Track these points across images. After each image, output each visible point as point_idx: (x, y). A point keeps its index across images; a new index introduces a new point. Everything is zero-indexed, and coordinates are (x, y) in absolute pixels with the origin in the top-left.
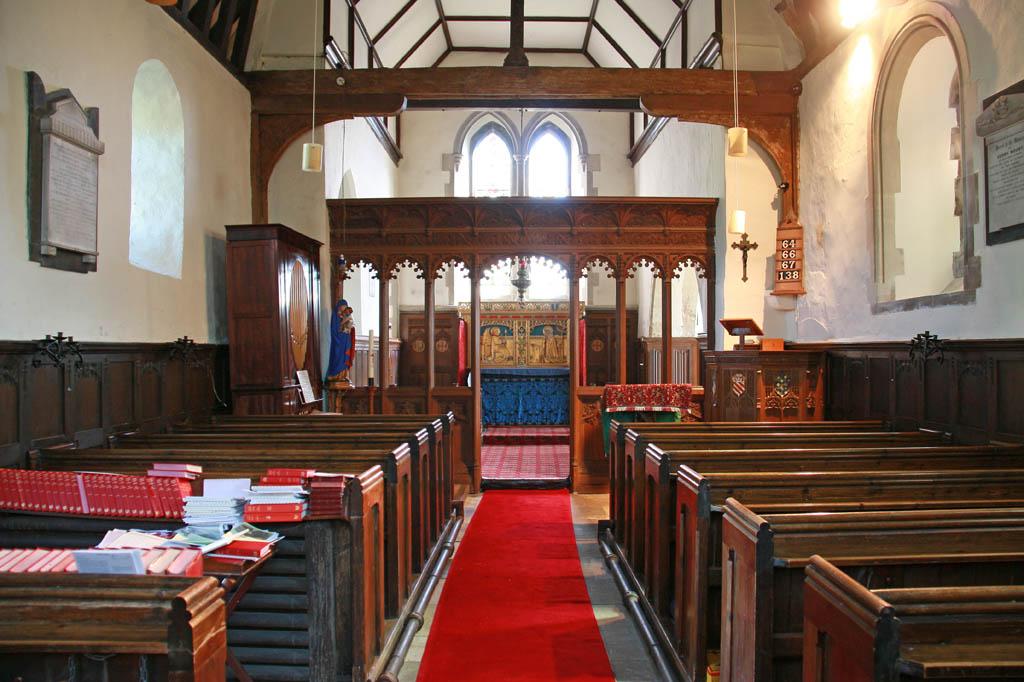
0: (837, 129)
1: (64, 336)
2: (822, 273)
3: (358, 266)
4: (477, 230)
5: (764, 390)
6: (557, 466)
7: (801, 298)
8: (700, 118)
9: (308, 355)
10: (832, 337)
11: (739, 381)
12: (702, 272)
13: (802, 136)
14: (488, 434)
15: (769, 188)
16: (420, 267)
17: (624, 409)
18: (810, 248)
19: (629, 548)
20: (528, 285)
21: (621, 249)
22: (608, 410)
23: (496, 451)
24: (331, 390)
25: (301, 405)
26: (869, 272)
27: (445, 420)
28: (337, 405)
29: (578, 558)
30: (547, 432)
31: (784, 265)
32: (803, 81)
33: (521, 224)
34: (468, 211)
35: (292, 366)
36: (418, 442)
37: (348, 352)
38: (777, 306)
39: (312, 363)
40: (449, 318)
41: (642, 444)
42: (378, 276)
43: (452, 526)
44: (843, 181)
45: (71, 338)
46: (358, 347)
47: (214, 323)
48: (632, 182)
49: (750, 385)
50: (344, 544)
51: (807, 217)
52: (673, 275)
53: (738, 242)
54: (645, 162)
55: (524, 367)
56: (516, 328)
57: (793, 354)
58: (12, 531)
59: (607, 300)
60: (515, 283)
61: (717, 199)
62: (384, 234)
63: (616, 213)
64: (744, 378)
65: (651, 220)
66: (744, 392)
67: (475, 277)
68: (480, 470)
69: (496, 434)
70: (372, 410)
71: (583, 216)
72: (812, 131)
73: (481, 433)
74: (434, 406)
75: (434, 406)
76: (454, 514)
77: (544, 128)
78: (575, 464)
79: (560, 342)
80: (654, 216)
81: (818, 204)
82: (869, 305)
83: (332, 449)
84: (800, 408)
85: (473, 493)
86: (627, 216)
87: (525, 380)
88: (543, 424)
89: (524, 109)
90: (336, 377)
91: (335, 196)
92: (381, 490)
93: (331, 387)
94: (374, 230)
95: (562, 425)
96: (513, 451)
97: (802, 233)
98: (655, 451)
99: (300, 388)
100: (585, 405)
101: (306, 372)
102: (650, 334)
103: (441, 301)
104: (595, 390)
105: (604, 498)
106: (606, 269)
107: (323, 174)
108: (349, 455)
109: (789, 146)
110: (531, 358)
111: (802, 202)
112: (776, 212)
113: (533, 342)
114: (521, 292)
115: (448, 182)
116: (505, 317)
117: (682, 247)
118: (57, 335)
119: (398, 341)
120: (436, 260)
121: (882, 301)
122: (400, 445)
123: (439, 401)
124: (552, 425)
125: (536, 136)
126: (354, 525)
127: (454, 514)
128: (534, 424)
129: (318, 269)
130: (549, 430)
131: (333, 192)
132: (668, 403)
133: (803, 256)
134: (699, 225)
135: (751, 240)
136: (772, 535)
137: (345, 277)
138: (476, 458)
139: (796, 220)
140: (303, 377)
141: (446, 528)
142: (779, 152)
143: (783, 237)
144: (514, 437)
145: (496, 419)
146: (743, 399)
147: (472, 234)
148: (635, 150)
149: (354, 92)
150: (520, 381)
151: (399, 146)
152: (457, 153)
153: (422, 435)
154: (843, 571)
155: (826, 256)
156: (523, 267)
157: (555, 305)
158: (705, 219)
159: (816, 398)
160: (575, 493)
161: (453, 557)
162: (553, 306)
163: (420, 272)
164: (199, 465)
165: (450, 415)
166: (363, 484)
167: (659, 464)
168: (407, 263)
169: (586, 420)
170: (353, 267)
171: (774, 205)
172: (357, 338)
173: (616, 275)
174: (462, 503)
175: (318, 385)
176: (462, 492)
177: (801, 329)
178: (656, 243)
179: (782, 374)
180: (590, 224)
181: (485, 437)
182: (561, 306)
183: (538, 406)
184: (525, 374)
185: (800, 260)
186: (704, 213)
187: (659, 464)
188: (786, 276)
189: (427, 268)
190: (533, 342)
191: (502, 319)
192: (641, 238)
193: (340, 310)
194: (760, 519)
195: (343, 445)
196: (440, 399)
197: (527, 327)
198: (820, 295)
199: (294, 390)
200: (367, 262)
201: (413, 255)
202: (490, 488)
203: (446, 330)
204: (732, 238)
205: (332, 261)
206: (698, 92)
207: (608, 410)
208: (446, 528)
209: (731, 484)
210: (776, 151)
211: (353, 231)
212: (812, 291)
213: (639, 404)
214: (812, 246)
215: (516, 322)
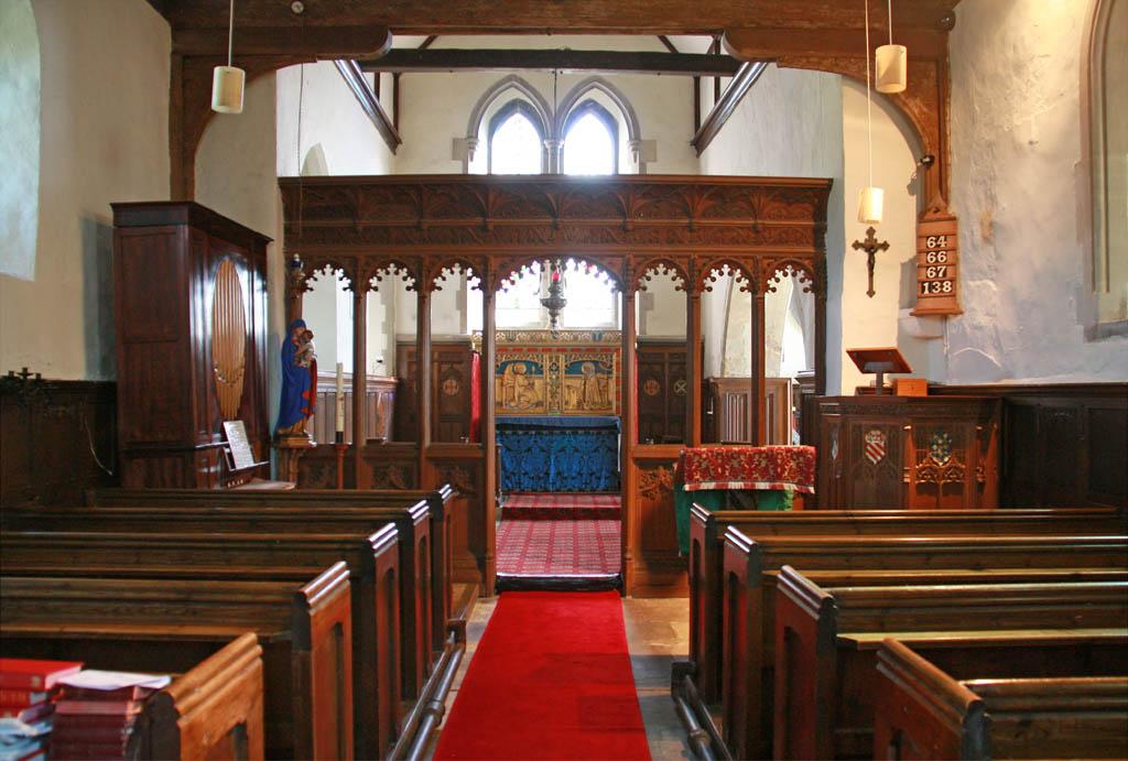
0: (1018, 68)
1: (29, 371)
2: (991, 283)
4: (492, 222)
5: (914, 455)
6: (602, 555)
7: (954, 321)
8: (808, 62)
9: (244, 399)
10: (1010, 376)
11: (874, 440)
12: (808, 283)
13: (954, 88)
14: (509, 506)
15: (904, 164)
16: (410, 274)
17: (711, 485)
18: (969, 246)
19: (730, 725)
20: (563, 306)
21: (698, 249)
22: (687, 487)
25: (230, 473)
26: (1080, 277)
28: (291, 470)
29: (643, 731)
30: (586, 502)
31: (931, 273)
32: (957, 9)
33: (553, 214)
34: (480, 198)
35: (213, 416)
36: (413, 520)
37: (306, 396)
39: (251, 410)
40: (455, 353)
42: (352, 287)
44: (1031, 143)
45: (38, 375)
46: (321, 388)
47: (97, 351)
48: (698, 166)
49: (893, 448)
51: (964, 198)
52: (767, 288)
53: (862, 241)
55: (557, 414)
56: (547, 365)
57: (946, 404)
59: (672, 327)
60: (546, 303)
61: (831, 180)
62: (360, 228)
64: (884, 437)
65: (736, 209)
66: (883, 458)
68: (494, 564)
69: (520, 505)
70: (341, 485)
71: (642, 202)
73: (497, 502)
74: (430, 472)
75: (430, 472)
76: (450, 641)
77: (584, 107)
79: (603, 383)
82: (1081, 328)
84: (966, 482)
85: (484, 596)
87: (558, 432)
88: (581, 490)
89: (558, 71)
90: (290, 429)
93: (283, 444)
95: (606, 491)
96: (542, 528)
97: (955, 226)
98: (739, 539)
99: (228, 446)
100: (642, 472)
101: (241, 422)
102: (722, 373)
103: (442, 326)
104: (653, 450)
106: (674, 279)
111: (954, 182)
112: (915, 197)
113: (569, 383)
114: (554, 315)
116: (532, 350)
117: (780, 249)
118: (21, 371)
119: (392, 380)
120: (433, 264)
121: (1104, 320)
122: (330, 565)
123: (437, 465)
124: (593, 492)
125: (573, 117)
127: (450, 641)
128: (570, 490)
129: (263, 275)
130: (589, 499)
132: (779, 477)
133: (957, 259)
134: (803, 217)
135: (880, 238)
138: (489, 546)
139: (946, 208)
140: (234, 432)
142: (922, 113)
143: (928, 233)
145: (520, 483)
147: (484, 228)
149: (316, 24)
150: (552, 434)
151: (397, 129)
152: (472, 137)
153: (419, 510)
154: (922, 656)
155: (998, 257)
156: (556, 281)
157: (597, 335)
158: (811, 209)
159: (987, 469)
160: (629, 597)
161: (441, 727)
162: (594, 336)
163: (410, 282)
165: (446, 492)
167: (705, 526)
168: (392, 268)
169: (645, 494)
170: (317, 273)
171: (911, 189)
173: (687, 287)
174: (464, 623)
175: (261, 441)
177: (952, 365)
178: (745, 242)
180: (649, 215)
181: (504, 508)
183: (575, 467)
184: (558, 424)
185: (954, 265)
187: (817, 617)
188: (932, 290)
189: (421, 275)
191: (527, 352)
193: (296, 334)
194: (823, 593)
196: (437, 461)
197: (562, 364)
198: (987, 314)
199: (217, 450)
201: (400, 257)
203: (455, 366)
204: (854, 232)
206: (806, 25)
207: (687, 487)
208: (437, 668)
211: (310, 223)
212: (974, 310)
213: (735, 478)
214: (973, 245)
215: (546, 356)
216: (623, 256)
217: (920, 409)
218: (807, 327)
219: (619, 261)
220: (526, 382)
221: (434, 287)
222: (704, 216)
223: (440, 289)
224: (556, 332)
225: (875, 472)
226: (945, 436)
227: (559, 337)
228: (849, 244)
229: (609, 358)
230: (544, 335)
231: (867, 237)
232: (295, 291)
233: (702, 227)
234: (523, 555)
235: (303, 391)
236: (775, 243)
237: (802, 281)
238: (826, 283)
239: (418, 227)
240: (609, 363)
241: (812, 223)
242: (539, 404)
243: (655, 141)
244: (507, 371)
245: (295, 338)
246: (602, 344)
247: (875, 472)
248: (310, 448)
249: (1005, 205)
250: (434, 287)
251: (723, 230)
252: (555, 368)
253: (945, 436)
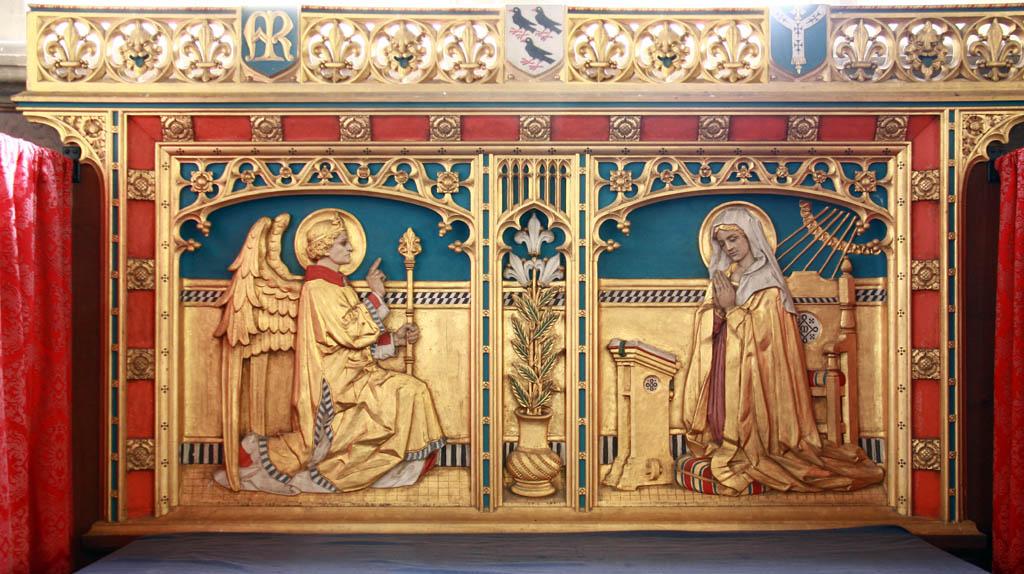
56: (487, 215)
58: (803, 347)
110: (609, 448)
116: (399, 123)
182: (859, 40)
190: (623, 324)
197: (581, 214)
218: (13, 90)
220: (365, 327)
229: (865, 177)
240: (865, 207)
242: (437, 457)
244: (248, 259)
246: (825, 87)
252: (533, 232)
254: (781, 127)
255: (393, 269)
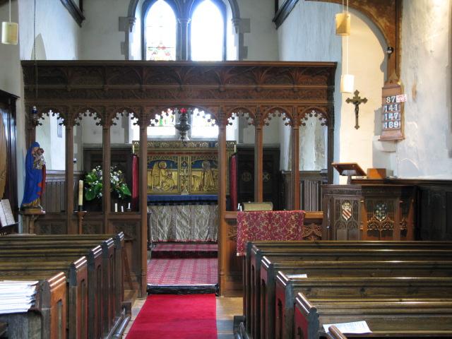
0: (428, 9)
2: (415, 124)
3: (48, 115)
4: (145, 86)
7: (400, 144)
11: (347, 208)
13: (404, 12)
14: (155, 250)
16: (99, 116)
23: (163, 263)
24: (26, 215)
27: (116, 239)
37: (40, 185)
38: (382, 149)
41: (260, 255)
43: (122, 321)
44: (431, 51)
48: (277, 46)
50: (36, 329)
54: (291, 24)
56: (180, 162)
61: (336, 63)
62: (69, 90)
63: (255, 74)
66: (351, 217)
67: (143, 124)
68: (146, 279)
72: (411, 9)
74: (111, 227)
76: (123, 312)
78: (222, 273)
80: (285, 76)
81: (414, 68)
83: (27, 261)
85: (140, 297)
86: (264, 76)
90: (30, 204)
91: (28, 57)
92: (64, 289)
93: (27, 212)
94: (62, 86)
98: (266, 261)
100: (230, 226)
103: (116, 139)
105: (239, 301)
107: (18, 46)
108: (41, 266)
109: (394, 21)
115: (124, 41)
123: (114, 224)
126: (44, 314)
127: (123, 312)
131: (27, 55)
134: (324, 85)
136: (318, 315)
137: (37, 123)
139: (398, 81)
141: (117, 323)
142: (386, 26)
144: (176, 252)
146: (351, 222)
147: (140, 90)
148: (280, 14)
153: (97, 250)
155: (419, 110)
160: (222, 297)
163: (98, 120)
164: (305, 273)
165: (121, 235)
166: (51, 285)
172: (47, 172)
176: (131, 296)
178: (287, 98)
179: (380, 203)
186: (326, 73)
191: (165, 154)
192: (274, 94)
193: (33, 150)
195: (36, 259)
197: (189, 162)
200: (55, 111)
202: (154, 293)
205: (26, 111)
208: (117, 323)
209: (310, 285)
210: (383, 25)
211: (46, 86)
216: (219, 106)
217: (368, 192)
219: (216, 108)
221: (112, 123)
222: (265, 83)
223: (115, 124)
224: (186, 142)
225: (347, 224)
226: (383, 206)
227: (189, 145)
228: (344, 98)
230: (177, 144)
231: (354, 96)
232: (31, 125)
233: (263, 90)
234: (163, 276)
235: (38, 183)
236: (304, 98)
237: (320, 119)
238: (334, 120)
239: (102, 90)
241: (326, 87)
242: (174, 187)
243: (249, 20)
245: (33, 153)
247: (347, 224)
248: (42, 215)
249: (421, 83)
250: (112, 123)
251: (274, 91)
253: (383, 206)
254: (210, 153)
255: (170, 168)
